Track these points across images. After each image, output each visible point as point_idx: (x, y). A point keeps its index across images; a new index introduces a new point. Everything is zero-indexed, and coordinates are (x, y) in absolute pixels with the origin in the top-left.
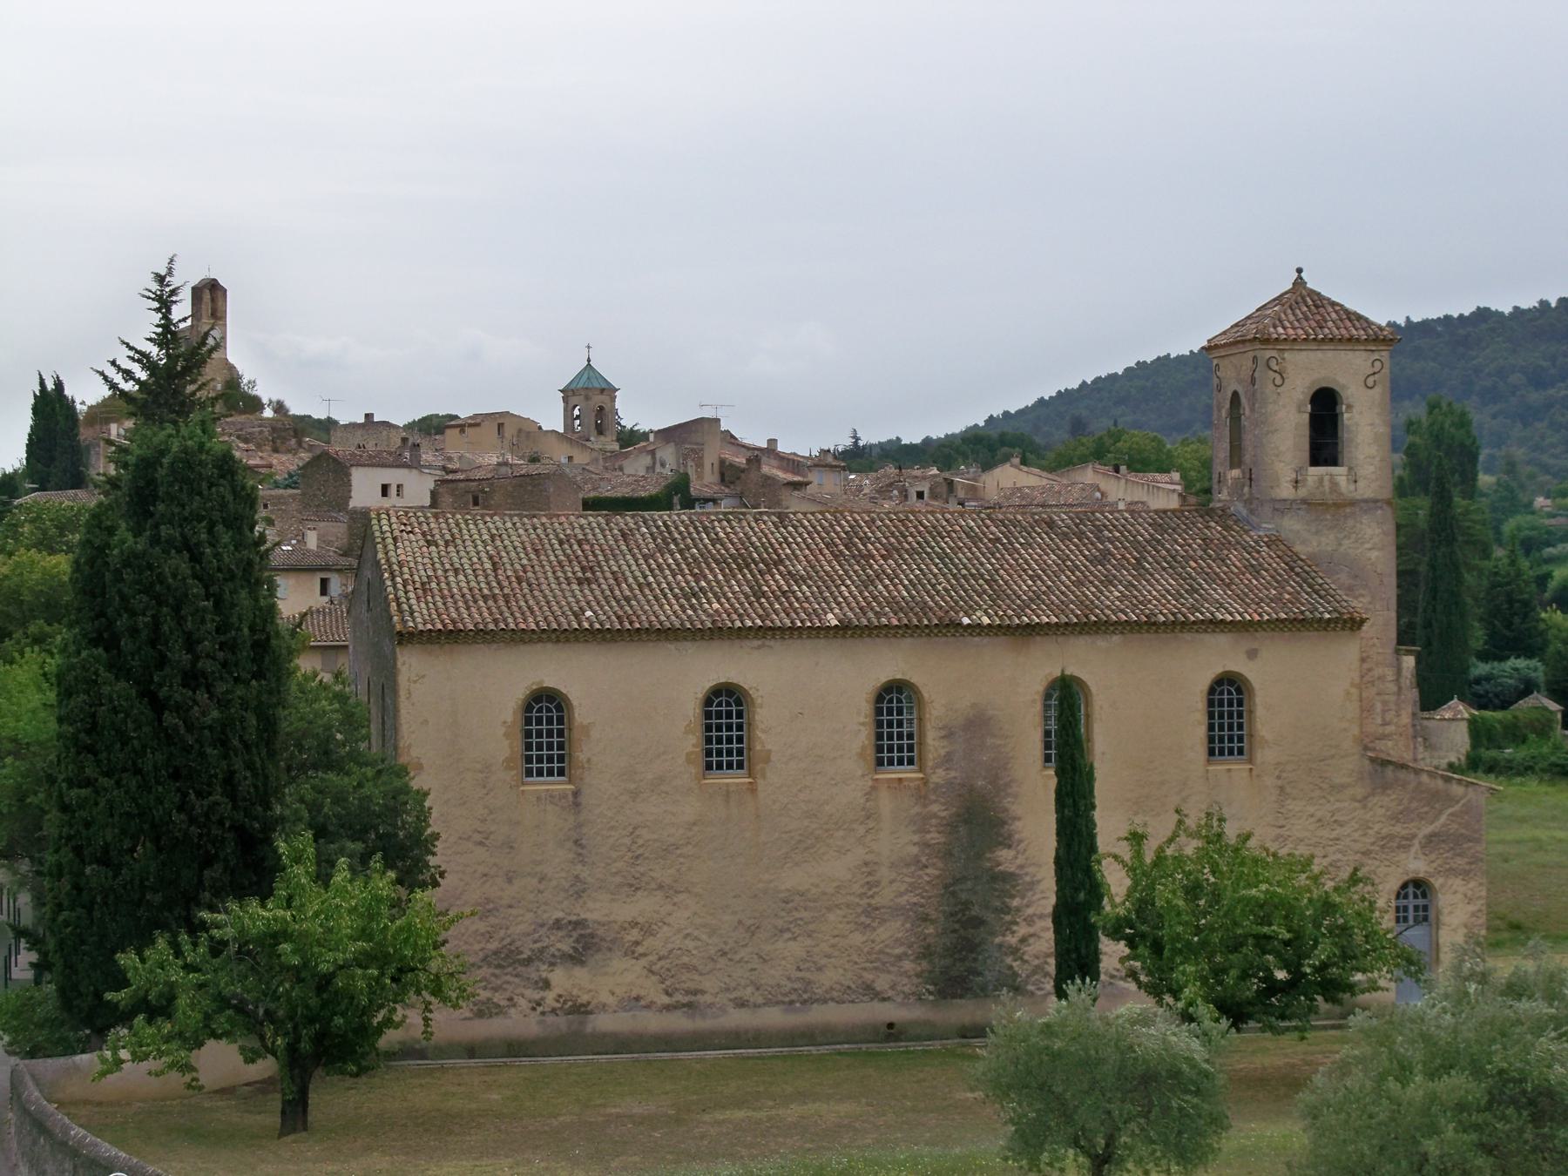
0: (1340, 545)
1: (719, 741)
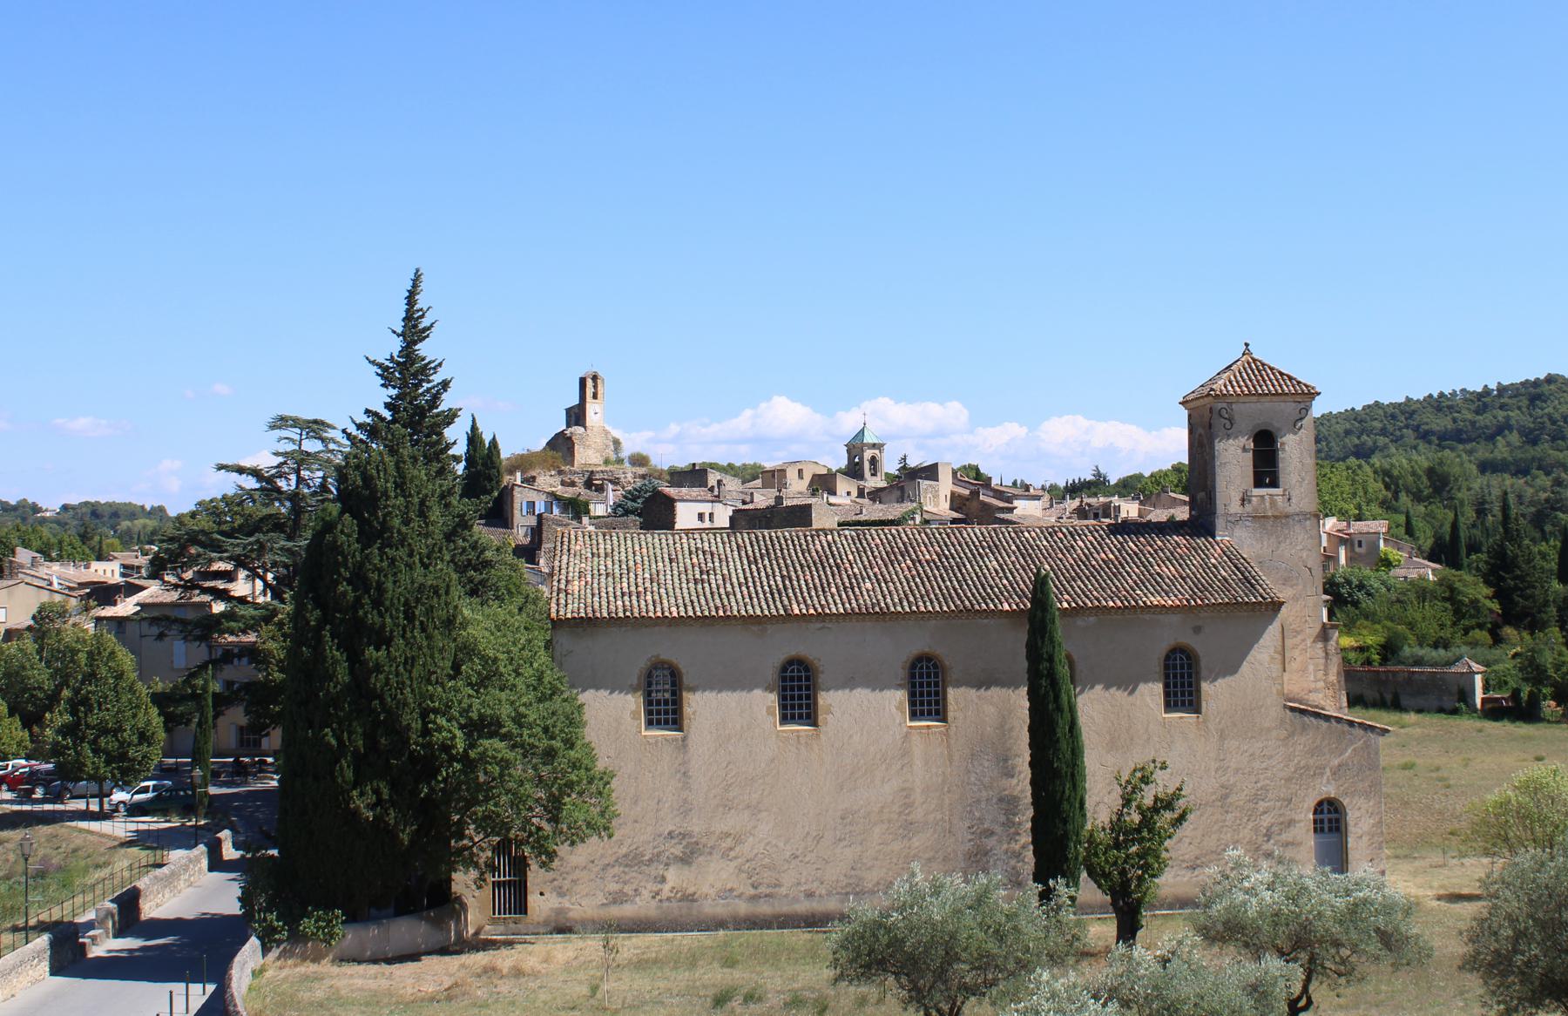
1: (792, 698)
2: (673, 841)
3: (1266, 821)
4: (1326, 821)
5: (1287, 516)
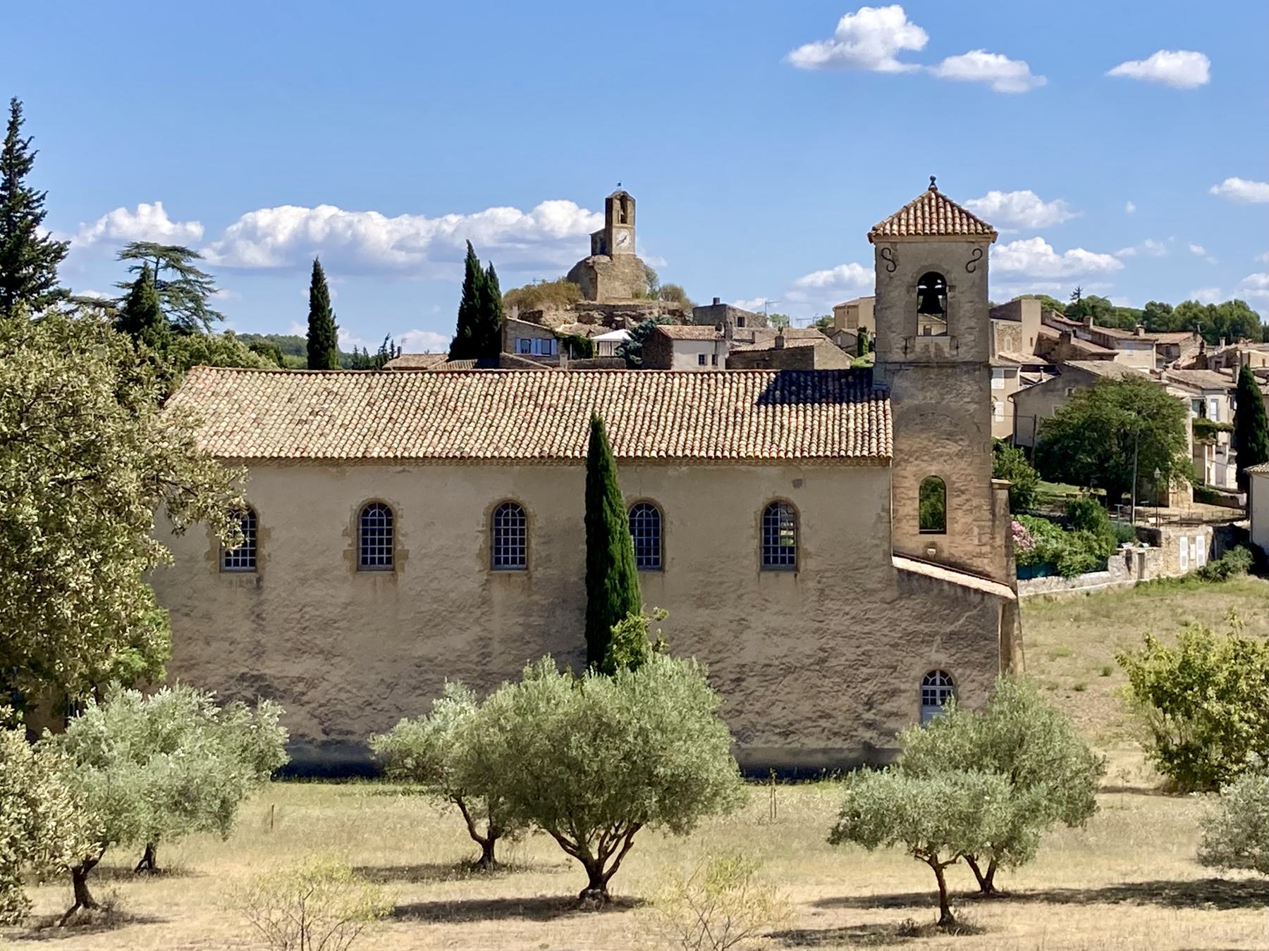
0: (943, 399)
2: (245, 684)
3: (869, 688)
4: (938, 693)
5: (954, 365)
